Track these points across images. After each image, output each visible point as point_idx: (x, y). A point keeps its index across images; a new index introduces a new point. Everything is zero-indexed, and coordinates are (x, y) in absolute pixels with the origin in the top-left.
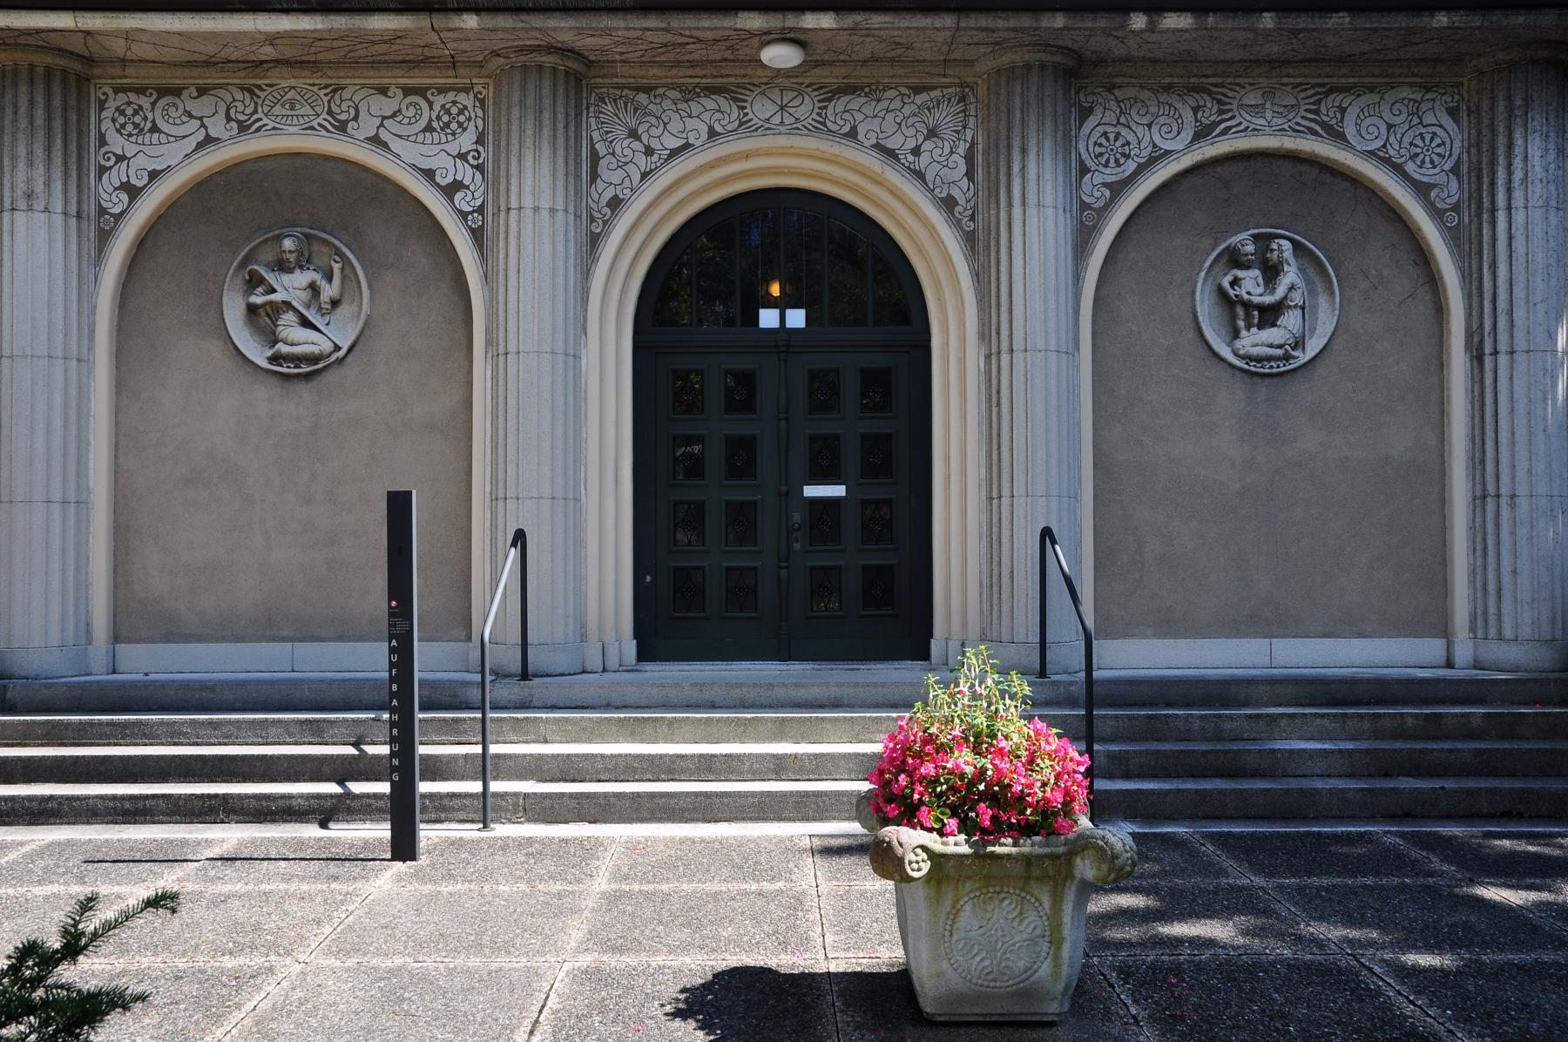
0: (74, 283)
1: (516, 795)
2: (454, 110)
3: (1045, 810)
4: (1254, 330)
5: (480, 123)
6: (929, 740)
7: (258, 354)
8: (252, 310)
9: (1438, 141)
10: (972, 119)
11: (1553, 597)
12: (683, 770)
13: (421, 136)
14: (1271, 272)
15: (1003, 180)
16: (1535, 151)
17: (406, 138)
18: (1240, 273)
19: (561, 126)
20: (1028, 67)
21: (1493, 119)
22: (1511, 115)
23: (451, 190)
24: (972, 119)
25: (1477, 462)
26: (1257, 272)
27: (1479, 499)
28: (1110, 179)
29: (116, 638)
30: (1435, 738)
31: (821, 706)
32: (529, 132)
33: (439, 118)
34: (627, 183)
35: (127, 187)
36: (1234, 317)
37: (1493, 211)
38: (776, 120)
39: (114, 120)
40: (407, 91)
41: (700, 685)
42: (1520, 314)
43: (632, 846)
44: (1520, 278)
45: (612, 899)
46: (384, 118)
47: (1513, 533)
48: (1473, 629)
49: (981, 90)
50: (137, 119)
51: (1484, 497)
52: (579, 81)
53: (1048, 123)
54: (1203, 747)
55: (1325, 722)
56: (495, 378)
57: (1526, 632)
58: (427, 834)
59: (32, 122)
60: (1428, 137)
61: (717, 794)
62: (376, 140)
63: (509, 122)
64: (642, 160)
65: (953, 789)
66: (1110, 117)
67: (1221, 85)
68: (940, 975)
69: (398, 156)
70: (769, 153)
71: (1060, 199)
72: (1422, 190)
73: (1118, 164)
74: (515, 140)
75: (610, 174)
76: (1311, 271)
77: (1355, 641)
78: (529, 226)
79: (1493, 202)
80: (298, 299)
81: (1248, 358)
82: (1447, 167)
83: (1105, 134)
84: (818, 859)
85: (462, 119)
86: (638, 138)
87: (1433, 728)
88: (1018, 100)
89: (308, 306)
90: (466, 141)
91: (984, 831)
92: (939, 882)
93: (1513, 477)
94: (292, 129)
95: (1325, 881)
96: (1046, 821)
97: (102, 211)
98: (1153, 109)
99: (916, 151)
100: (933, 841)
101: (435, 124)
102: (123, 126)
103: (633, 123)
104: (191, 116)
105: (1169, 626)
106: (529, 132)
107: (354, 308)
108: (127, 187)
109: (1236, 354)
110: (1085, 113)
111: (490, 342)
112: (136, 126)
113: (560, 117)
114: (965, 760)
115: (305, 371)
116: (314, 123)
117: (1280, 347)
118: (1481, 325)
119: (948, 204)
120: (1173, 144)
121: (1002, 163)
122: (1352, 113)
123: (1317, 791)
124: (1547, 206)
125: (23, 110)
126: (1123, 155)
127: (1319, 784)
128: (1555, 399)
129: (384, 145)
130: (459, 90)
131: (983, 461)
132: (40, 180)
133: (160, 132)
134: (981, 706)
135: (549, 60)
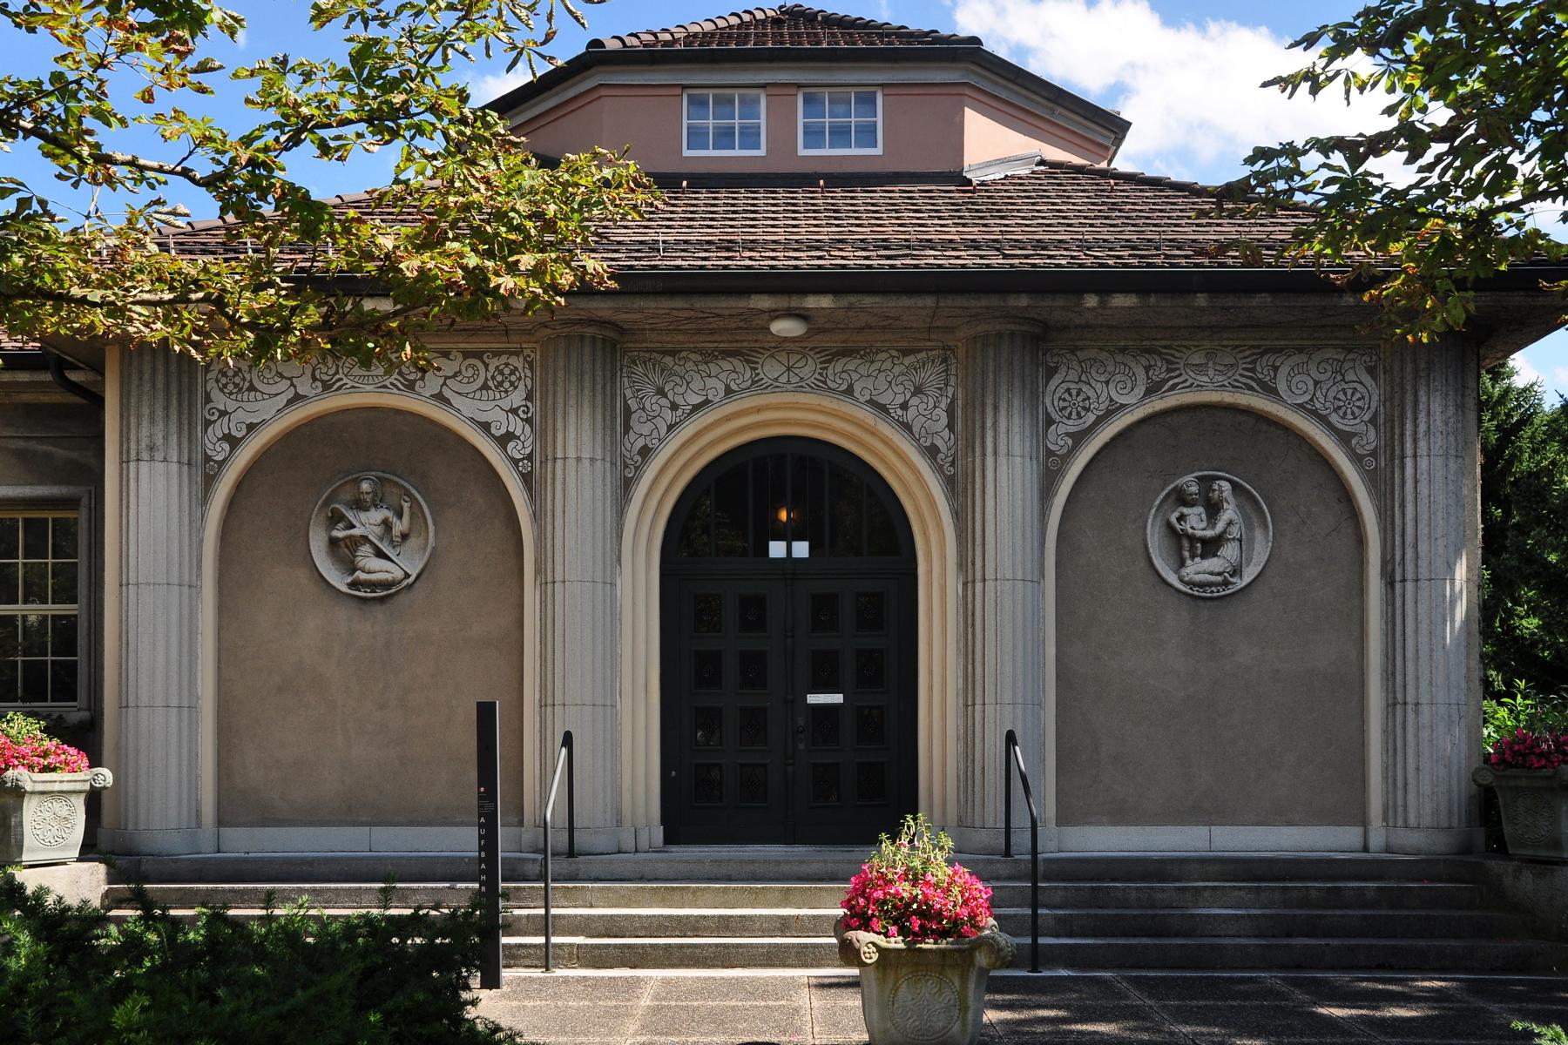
0: (186, 521)
1: (571, 945)
2: (507, 371)
3: (956, 920)
4: (1198, 559)
5: (529, 382)
6: (882, 876)
7: (339, 581)
8: (333, 543)
9: (1358, 395)
10: (953, 379)
11: (1450, 791)
12: (706, 928)
13: (478, 395)
14: (1213, 509)
15: (978, 432)
16: (1436, 407)
17: (466, 395)
18: (1185, 510)
19: (599, 387)
20: (1000, 335)
21: (1402, 378)
22: (1416, 377)
23: (504, 440)
24: (953, 379)
25: (1389, 674)
26: (1201, 509)
27: (1391, 705)
28: (1073, 429)
29: (220, 822)
30: (1335, 907)
31: (820, 880)
32: (572, 393)
33: (493, 378)
34: (655, 434)
35: (228, 438)
36: (1180, 548)
37: (1403, 457)
38: (784, 379)
39: (217, 381)
40: (467, 354)
41: (720, 862)
42: (1423, 547)
43: (666, 982)
44: (1424, 517)
45: (656, 1010)
46: (447, 378)
47: (1417, 736)
48: (1385, 819)
49: (961, 353)
50: (237, 380)
51: (1395, 705)
52: (614, 344)
53: (1017, 384)
54: (1135, 912)
55: (1242, 893)
56: (543, 602)
57: (1427, 820)
58: (506, 974)
59: (154, 386)
60: (1349, 392)
61: (733, 945)
62: (440, 398)
63: (555, 383)
64: (668, 415)
65: (895, 907)
66: (1073, 376)
67: (1170, 347)
68: (886, 1031)
69: (458, 411)
70: (776, 408)
71: (1027, 449)
72: (1344, 438)
73: (1079, 416)
74: (560, 400)
75: (640, 427)
76: (1248, 508)
77: (1285, 829)
78: (573, 473)
79: (1402, 449)
80: (374, 533)
81: (1191, 584)
82: (1366, 418)
83: (1068, 390)
84: (813, 990)
85: (513, 378)
86: (665, 395)
87: (1333, 898)
88: (991, 363)
89: (381, 539)
90: (517, 398)
91: (915, 934)
92: (885, 968)
93: (1417, 688)
94: (368, 388)
95: (1202, 1003)
96: (954, 929)
97: (208, 459)
98: (1111, 369)
99: (904, 406)
100: (881, 941)
101: (490, 383)
102: (225, 386)
103: (660, 382)
104: (282, 377)
105: (1121, 815)
106: (572, 393)
107: (421, 541)
108: (228, 438)
109: (1181, 580)
110: (1051, 372)
111: (539, 571)
112: (236, 385)
113: (599, 379)
114: (905, 890)
115: (382, 594)
116: (387, 383)
117: (1220, 574)
118: (1393, 555)
119: (932, 452)
120: (1126, 399)
121: (978, 417)
122: (1284, 371)
123: (1225, 947)
124: (1446, 455)
125: (146, 376)
126: (1084, 408)
127: (1227, 941)
128: (1453, 621)
129: (447, 402)
130: (511, 354)
131: (961, 674)
132: (160, 435)
133: (256, 390)
134: (923, 859)
135: (589, 331)
